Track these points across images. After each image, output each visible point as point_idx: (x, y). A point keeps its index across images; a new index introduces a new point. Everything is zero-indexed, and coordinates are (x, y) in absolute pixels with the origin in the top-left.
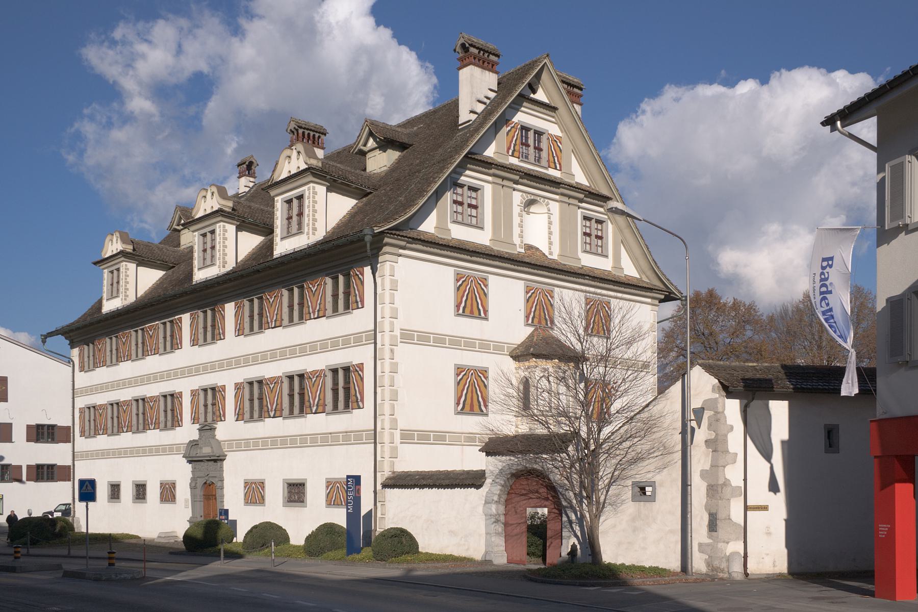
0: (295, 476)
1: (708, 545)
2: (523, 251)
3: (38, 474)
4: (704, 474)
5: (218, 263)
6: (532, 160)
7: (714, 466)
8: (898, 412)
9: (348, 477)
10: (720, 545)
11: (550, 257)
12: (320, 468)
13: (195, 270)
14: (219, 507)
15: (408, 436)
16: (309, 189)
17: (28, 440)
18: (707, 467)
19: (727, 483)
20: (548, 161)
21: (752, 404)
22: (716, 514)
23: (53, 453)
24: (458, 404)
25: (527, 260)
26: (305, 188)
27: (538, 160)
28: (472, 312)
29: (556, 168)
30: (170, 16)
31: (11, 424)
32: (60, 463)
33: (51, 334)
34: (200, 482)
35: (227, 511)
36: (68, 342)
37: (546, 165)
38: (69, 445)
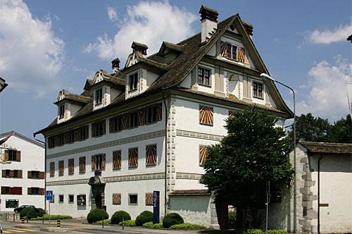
0: (133, 193)
1: (302, 221)
7: (306, 186)
8: (41, 180)
12: (143, 189)
18: (303, 187)
19: (311, 194)
21: (322, 160)
23: (39, 183)
27: (235, 58)
30: (38, 21)
32: (40, 187)
33: (37, 133)
38: (44, 180)
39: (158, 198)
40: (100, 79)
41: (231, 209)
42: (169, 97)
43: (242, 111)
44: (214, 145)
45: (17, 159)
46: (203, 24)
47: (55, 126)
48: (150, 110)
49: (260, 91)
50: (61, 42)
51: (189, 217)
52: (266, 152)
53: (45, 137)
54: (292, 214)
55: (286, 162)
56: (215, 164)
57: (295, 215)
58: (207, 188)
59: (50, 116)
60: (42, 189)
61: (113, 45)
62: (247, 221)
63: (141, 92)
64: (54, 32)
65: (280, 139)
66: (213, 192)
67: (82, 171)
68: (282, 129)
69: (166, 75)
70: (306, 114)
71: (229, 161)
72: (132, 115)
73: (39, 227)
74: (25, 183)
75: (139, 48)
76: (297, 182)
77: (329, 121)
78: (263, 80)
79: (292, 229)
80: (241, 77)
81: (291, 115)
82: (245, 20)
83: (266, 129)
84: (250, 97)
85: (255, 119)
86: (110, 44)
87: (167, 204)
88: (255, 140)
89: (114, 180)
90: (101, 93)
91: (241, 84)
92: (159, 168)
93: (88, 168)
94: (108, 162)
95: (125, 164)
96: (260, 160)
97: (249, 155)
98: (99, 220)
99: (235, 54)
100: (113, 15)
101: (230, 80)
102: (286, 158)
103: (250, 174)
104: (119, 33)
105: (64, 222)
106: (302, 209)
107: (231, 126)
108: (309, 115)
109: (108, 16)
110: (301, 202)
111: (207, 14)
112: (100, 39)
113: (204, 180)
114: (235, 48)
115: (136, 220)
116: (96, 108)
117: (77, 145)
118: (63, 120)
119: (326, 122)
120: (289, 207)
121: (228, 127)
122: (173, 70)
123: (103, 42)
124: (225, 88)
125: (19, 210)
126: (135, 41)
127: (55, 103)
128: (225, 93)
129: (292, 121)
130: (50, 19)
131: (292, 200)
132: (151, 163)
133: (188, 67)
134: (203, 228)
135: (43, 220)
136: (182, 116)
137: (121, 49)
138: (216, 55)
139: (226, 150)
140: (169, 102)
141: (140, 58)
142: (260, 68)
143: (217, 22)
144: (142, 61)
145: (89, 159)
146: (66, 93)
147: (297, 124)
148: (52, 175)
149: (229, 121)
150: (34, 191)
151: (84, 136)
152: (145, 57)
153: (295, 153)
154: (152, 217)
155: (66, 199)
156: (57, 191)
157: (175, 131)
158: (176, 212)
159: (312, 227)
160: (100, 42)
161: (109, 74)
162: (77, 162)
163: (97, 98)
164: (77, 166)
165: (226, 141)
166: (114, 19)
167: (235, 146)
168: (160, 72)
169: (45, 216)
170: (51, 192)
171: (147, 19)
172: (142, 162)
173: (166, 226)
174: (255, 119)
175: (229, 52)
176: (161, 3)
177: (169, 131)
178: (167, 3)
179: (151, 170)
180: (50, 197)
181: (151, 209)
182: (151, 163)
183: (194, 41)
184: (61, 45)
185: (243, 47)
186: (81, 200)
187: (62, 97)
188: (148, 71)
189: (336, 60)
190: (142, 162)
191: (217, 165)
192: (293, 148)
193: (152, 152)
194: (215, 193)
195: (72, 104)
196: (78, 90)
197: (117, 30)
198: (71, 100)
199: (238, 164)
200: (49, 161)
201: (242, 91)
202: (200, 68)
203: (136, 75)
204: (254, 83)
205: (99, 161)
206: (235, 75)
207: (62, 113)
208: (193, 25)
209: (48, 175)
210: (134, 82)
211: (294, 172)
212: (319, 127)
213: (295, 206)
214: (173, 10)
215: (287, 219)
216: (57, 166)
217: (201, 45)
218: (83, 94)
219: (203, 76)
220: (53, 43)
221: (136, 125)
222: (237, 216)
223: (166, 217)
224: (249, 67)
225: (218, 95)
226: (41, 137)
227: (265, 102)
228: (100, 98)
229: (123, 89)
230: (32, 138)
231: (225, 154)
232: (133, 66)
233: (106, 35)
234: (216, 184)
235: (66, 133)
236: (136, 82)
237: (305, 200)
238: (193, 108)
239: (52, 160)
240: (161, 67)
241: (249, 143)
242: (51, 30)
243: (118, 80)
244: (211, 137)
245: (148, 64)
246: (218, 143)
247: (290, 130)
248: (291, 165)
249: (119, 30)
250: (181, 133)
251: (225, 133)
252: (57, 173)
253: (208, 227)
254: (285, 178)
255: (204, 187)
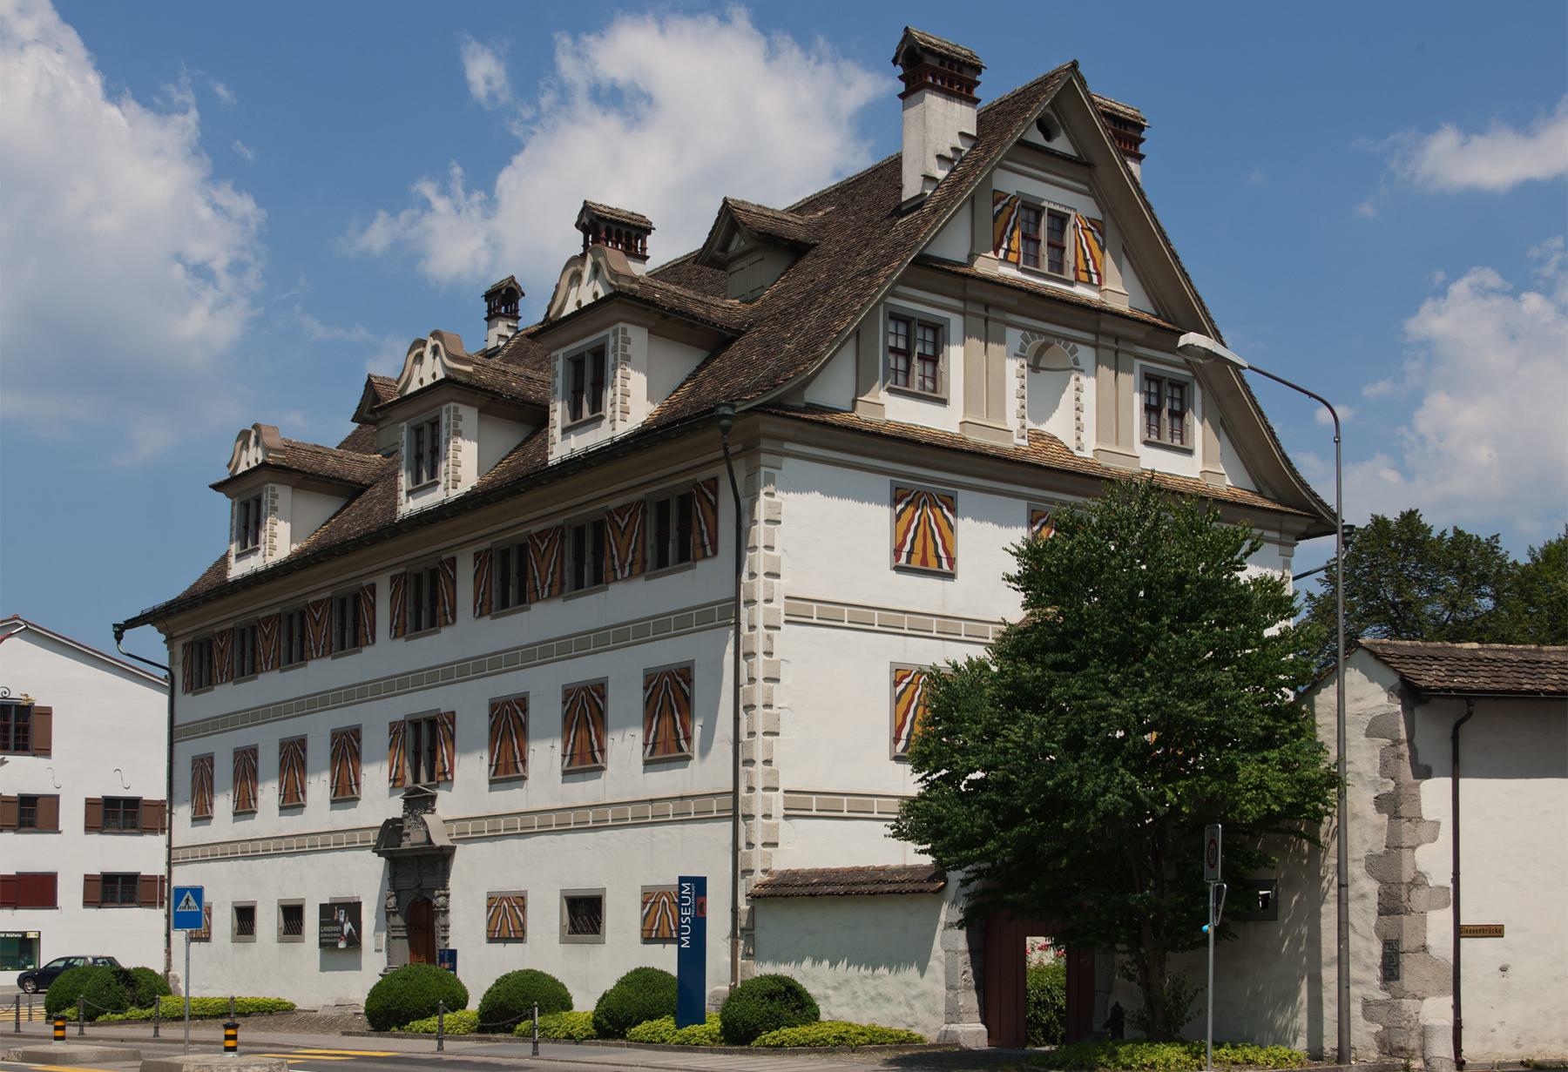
0: (583, 884)
1: (1380, 1004)
2: (1025, 442)
3: (105, 891)
4: (1374, 865)
5: (443, 481)
6: (1045, 269)
7: (1394, 846)
9: (682, 879)
10: (1407, 1003)
11: (1077, 453)
12: (627, 868)
13: (403, 495)
14: (440, 945)
15: (800, 806)
16: (615, 333)
17: (359, 968)
19: (1418, 881)
20: (1076, 269)
22: (1397, 941)
23: (138, 854)
24: (896, 740)
25: (1033, 459)
26: (609, 331)
27: (1058, 265)
28: (924, 561)
29: (1090, 282)
31: (57, 797)
32: (145, 871)
33: (132, 623)
34: (723, 1046)
35: (454, 952)
36: (163, 637)
37: (1072, 277)
38: (162, 839)
39: (701, 908)
40: (430, 371)
41: (1041, 953)
42: (751, 449)
43: (1091, 508)
44: (962, 662)
45: (34, 741)
46: (911, 113)
47: (214, 591)
48: (663, 508)
49: (1178, 415)
50: (244, 205)
51: (846, 993)
52: (1201, 691)
53: (170, 641)
54: (1329, 975)
55: (1296, 734)
56: (962, 750)
57: (1344, 981)
58: (928, 860)
59: (195, 544)
60: (151, 880)
61: (487, 216)
62: (1118, 1012)
63: (623, 428)
64: (208, 161)
65: (1269, 632)
66: (955, 876)
67: (345, 793)
68: (1278, 587)
69: (735, 351)
70: (1393, 515)
71: (1028, 735)
72: (201, 645)
73: (136, 1056)
74: (73, 854)
75: (610, 230)
76: (1352, 828)
77: (1504, 545)
78: (1188, 365)
79: (1330, 1043)
80: (1086, 354)
81: (1319, 520)
82: (1109, 90)
83: (1205, 586)
84: (1131, 445)
85: (1152, 541)
86: (476, 213)
87: (744, 934)
88: (1153, 637)
89: (493, 830)
90: (435, 436)
91: (1089, 383)
92: (707, 772)
93: (375, 777)
94: (468, 751)
95: (545, 755)
96: (1175, 729)
97: (1124, 707)
98: (423, 1016)
99: (1058, 247)
100: (489, 81)
101: (1035, 368)
102: (1296, 719)
103: (1131, 796)
104: (518, 160)
105: (258, 1028)
106: (1377, 949)
107: (1039, 575)
108: (1410, 518)
109: (463, 85)
110: (1373, 918)
111: (928, 68)
112: (428, 189)
113: (916, 821)
114: (1060, 220)
115: (597, 1013)
116: (409, 506)
117: (322, 673)
118: (254, 563)
119: (1489, 549)
120: (1315, 940)
121: (1026, 581)
122: (768, 332)
123: (441, 204)
124: (1012, 404)
125: (42, 979)
126: (598, 199)
127: (217, 487)
128: (1010, 429)
129: (1324, 548)
130: (190, 98)
131: (1329, 911)
132: (667, 749)
133: (836, 311)
134: (907, 1041)
135: (157, 1020)
136: (814, 535)
137: (525, 229)
138: (972, 257)
139: (1017, 685)
140: (752, 473)
141: (616, 275)
142: (1175, 306)
143: (976, 101)
144: (624, 289)
145: (375, 738)
146: (266, 440)
147: (1353, 560)
148: (202, 815)
149: (1032, 554)
150: (113, 890)
151: (351, 632)
152: (638, 269)
153: (1341, 694)
154: (672, 994)
155: (268, 922)
156: (222, 887)
157: (779, 605)
158: (784, 970)
159: (1424, 1033)
160: (426, 205)
161: (471, 348)
162: (319, 751)
163: (419, 457)
164: (319, 771)
165: (1017, 644)
166: (492, 97)
167: (1057, 666)
168: (716, 340)
169: (166, 1003)
170: (198, 893)
171: (648, 99)
172: (625, 746)
173: (738, 1034)
174: (1152, 541)
175: (1030, 239)
176: (713, 22)
177: (751, 602)
178: (741, 17)
179: (667, 782)
180: (189, 915)
181: (665, 959)
182: (667, 749)
183: (870, 196)
184: (244, 221)
185: (1097, 214)
186: (340, 926)
187: (252, 457)
188: (483, 411)
189: (1541, 262)
190: (625, 746)
191: (976, 752)
192: (1330, 673)
193: (671, 704)
194: (965, 883)
195: (296, 487)
196: (324, 425)
197: (508, 150)
198: (293, 472)
199: (1074, 745)
200: (189, 750)
201: (1091, 418)
202: (895, 317)
203: (599, 354)
204: (1149, 377)
205: (424, 746)
206: (1059, 346)
207: (248, 530)
208: (867, 121)
209: (182, 814)
210: (590, 385)
211: (1335, 780)
212: (1457, 574)
213: (1343, 938)
214: (772, 54)
215: (1304, 994)
216: (224, 770)
217: (900, 211)
218: (351, 443)
219: (907, 354)
220: (205, 213)
221: (600, 580)
222: (1068, 988)
223: (735, 995)
224: (1123, 306)
225: (976, 438)
226: (150, 642)
227: (1199, 462)
228: (428, 459)
229: (537, 419)
230: (107, 645)
231: (1011, 703)
232: (582, 312)
233: (458, 171)
234: (969, 842)
235: (267, 620)
236: (599, 385)
237: (1391, 906)
238: (842, 496)
239: (201, 746)
240: (717, 315)
241: (1124, 652)
242: (195, 153)
243: (514, 378)
244: (947, 627)
245: (652, 303)
246: (979, 653)
247: (1319, 591)
248: (1321, 747)
249: (518, 147)
250: (803, 612)
251: (1012, 608)
252: (223, 804)
253: (931, 1037)
254: (1294, 810)
255: (911, 856)
